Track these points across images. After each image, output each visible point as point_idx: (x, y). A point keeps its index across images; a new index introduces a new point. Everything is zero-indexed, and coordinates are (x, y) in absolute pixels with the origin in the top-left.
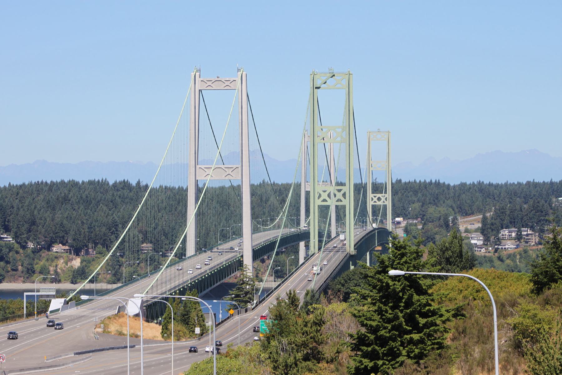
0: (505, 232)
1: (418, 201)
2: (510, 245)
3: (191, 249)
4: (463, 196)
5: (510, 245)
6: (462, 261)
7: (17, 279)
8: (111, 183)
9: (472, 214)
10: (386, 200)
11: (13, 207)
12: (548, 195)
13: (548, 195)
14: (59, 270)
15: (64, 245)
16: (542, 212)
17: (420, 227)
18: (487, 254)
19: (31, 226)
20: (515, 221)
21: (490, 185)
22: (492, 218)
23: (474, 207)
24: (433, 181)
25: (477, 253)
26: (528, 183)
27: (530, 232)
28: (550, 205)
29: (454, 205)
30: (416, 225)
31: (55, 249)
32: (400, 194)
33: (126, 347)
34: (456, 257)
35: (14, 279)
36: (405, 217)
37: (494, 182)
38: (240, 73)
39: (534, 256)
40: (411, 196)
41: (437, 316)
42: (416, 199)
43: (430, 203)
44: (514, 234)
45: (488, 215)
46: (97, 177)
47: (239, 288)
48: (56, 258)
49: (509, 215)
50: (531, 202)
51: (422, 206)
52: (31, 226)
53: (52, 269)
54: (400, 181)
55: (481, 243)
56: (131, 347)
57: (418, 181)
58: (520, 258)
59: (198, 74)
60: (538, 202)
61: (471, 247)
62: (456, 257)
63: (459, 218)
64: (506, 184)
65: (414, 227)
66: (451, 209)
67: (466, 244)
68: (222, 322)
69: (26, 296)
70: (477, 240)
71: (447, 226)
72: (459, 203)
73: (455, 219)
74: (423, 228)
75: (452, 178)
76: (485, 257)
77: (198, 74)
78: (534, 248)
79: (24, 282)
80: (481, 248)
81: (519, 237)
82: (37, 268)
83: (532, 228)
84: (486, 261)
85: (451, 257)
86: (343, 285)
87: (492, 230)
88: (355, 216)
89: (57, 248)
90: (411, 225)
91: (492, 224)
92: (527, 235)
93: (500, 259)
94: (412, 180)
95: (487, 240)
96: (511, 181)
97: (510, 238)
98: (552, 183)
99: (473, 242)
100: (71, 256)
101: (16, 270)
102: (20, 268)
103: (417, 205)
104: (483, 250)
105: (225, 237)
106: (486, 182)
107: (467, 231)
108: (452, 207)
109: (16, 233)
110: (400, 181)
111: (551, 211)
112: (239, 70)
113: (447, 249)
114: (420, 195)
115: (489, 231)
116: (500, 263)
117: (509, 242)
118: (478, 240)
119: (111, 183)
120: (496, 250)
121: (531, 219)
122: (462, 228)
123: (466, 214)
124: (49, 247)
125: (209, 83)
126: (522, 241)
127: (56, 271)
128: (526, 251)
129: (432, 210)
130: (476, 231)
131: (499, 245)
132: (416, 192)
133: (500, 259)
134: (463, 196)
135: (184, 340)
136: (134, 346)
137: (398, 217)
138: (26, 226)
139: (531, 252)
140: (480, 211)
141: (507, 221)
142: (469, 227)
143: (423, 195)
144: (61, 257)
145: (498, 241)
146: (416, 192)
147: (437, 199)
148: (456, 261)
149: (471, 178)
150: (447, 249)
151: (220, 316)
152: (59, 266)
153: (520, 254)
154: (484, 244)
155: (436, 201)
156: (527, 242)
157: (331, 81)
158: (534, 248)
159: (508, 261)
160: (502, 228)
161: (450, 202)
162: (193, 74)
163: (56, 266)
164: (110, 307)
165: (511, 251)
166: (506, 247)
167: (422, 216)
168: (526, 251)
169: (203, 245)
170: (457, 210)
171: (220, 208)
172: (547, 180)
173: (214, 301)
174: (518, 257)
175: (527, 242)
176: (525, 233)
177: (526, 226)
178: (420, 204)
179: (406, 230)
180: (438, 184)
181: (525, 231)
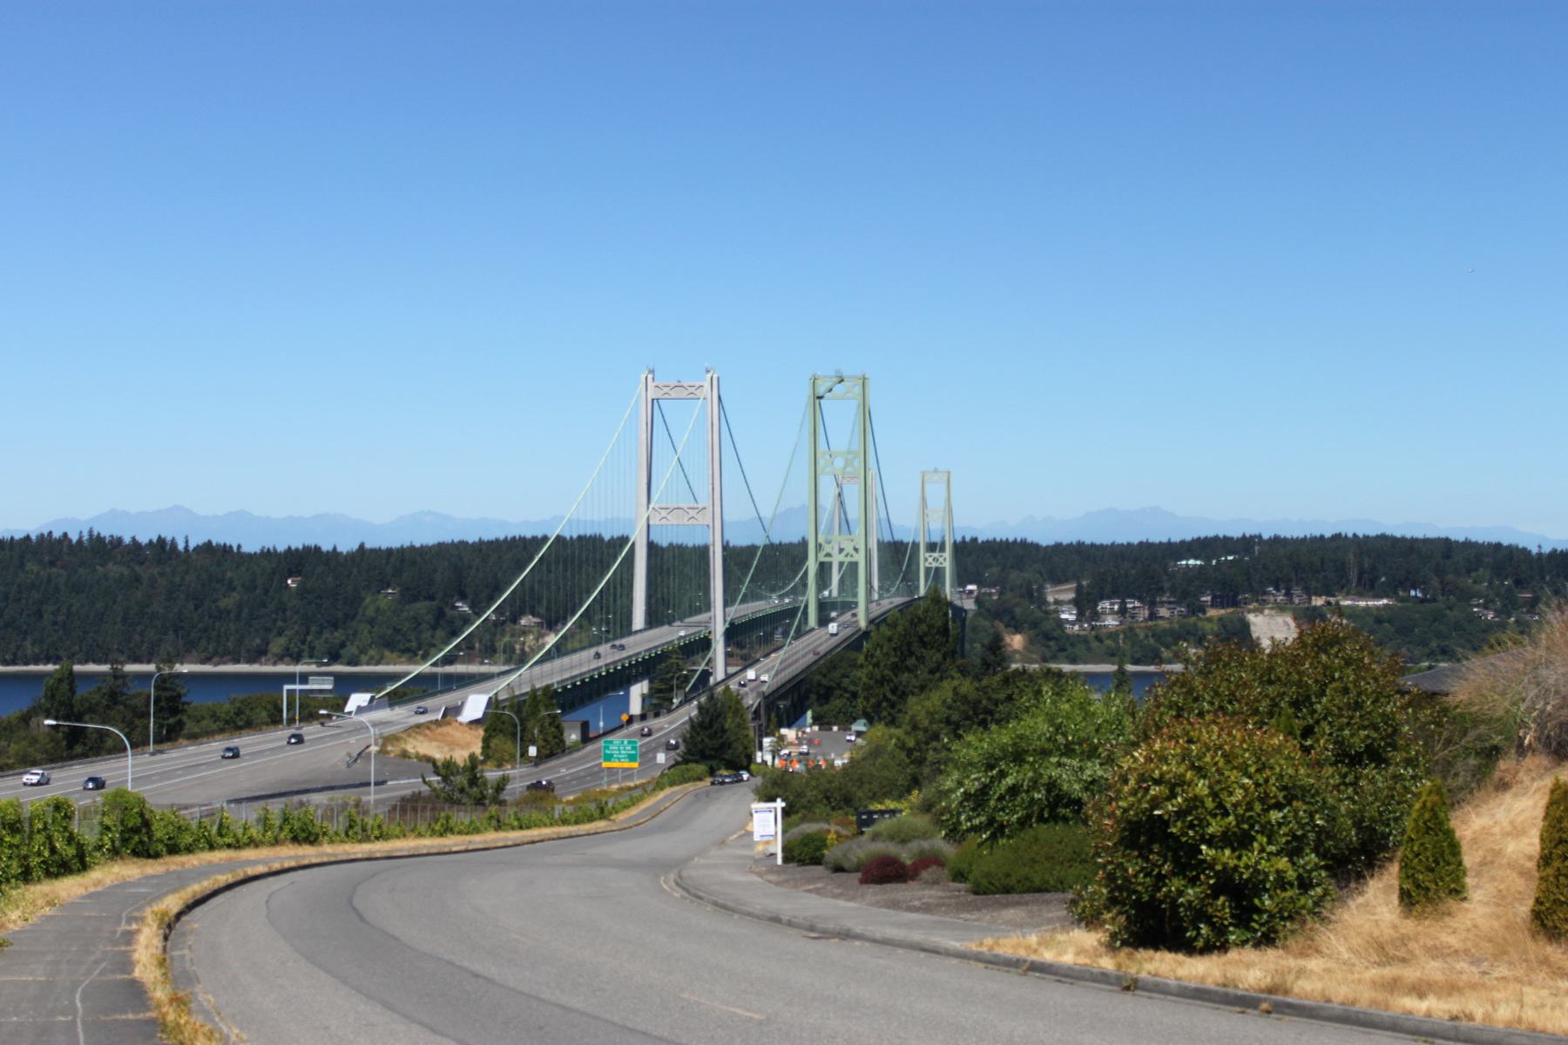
0: (1105, 605)
2: (1111, 622)
3: (639, 620)
5: (1111, 622)
10: (946, 560)
27: (1137, 604)
31: (523, 622)
33: (369, 784)
37: (1098, 542)
39: (1142, 636)
40: (976, 557)
41: (117, 843)
63: (1251, 617)
70: (1068, 615)
71: (1030, 595)
75: (1044, 537)
81: (1123, 611)
82: (500, 645)
83: (1140, 599)
85: (926, 634)
95: (1080, 615)
97: (1112, 612)
99: (1063, 616)
103: (995, 570)
105: (699, 611)
106: (1088, 541)
107: (1057, 602)
113: (921, 620)
115: (1085, 604)
120: (1093, 628)
122: (1050, 599)
124: (515, 620)
128: (1131, 629)
129: (1015, 577)
130: (1069, 602)
136: (383, 783)
145: (1096, 616)
150: (921, 620)
155: (1020, 564)
159: (1108, 642)
160: (1102, 599)
167: (1000, 582)
168: (1131, 629)
169: (653, 620)
171: (677, 569)
172: (1164, 540)
173: (1442, 664)
177: (1133, 596)
180: (1024, 544)
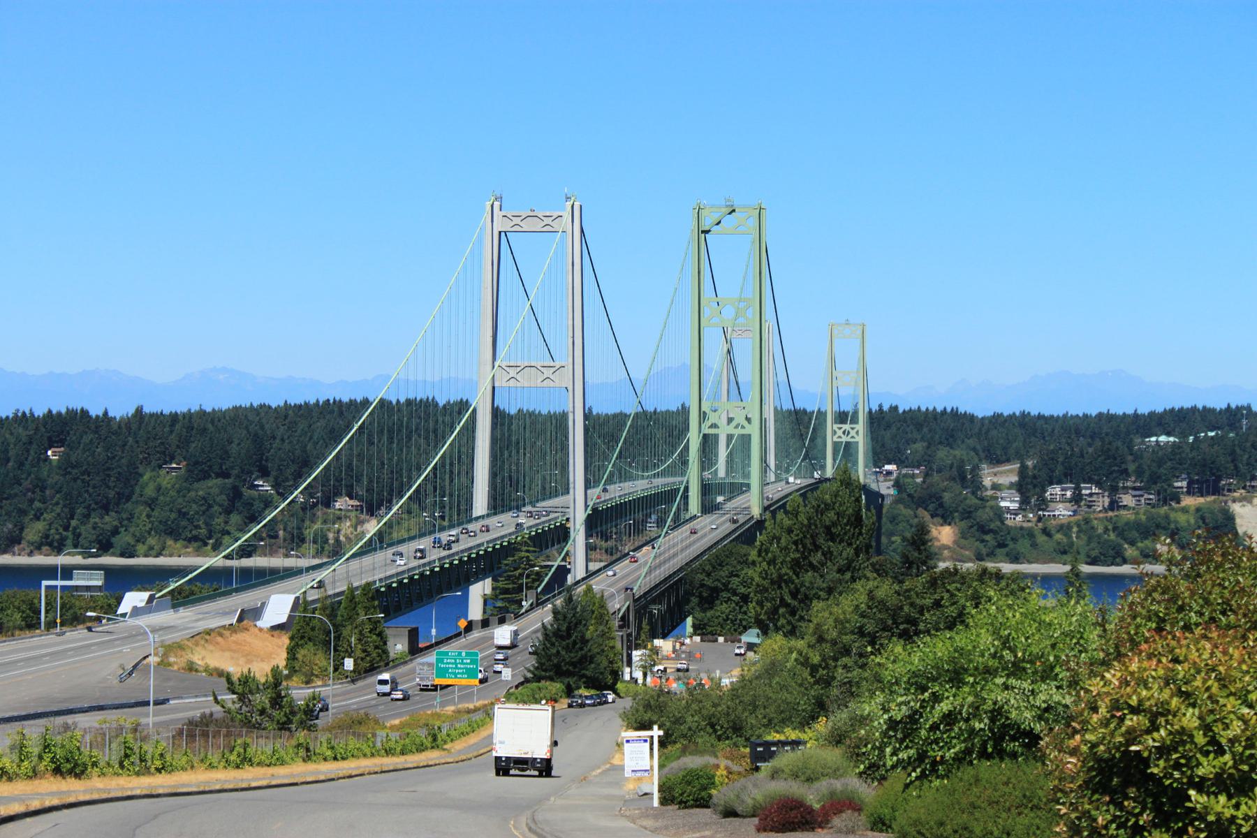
0: (1055, 490)
1: (922, 439)
2: (1062, 511)
4: (994, 433)
5: (1062, 511)
6: (860, 534)
7: (276, 552)
8: (441, 403)
9: (1008, 461)
10: (859, 434)
11: (274, 438)
12: (1128, 433)
13: (1128, 433)
14: (342, 538)
15: (351, 498)
16: (1115, 459)
17: (919, 480)
18: (1025, 525)
19: (301, 468)
20: (1072, 473)
21: (1040, 417)
22: (1035, 467)
23: (1011, 451)
24: (949, 410)
25: (1009, 523)
26: (1100, 415)
27: (1095, 490)
28: (1130, 448)
29: (978, 447)
30: (913, 476)
31: (338, 505)
32: (894, 429)
34: (846, 525)
35: (272, 553)
36: (900, 463)
38: (569, 204)
40: (894, 430)
42: (919, 437)
43: (941, 443)
44: (1069, 494)
45: (1030, 463)
46: (420, 394)
47: (509, 577)
48: (339, 518)
49: (1063, 463)
50: (1098, 443)
51: (928, 447)
52: (301, 468)
53: (331, 535)
54: (896, 408)
55: (1016, 506)
56: (157, 703)
57: (923, 409)
58: (1079, 532)
59: (497, 204)
60: (1110, 443)
61: (999, 513)
62: (846, 525)
63: (1236, 508)
64: (1065, 416)
65: (909, 480)
66: (973, 453)
67: (992, 507)
68: (438, 644)
69: (47, 587)
70: (1009, 502)
71: (963, 478)
72: (986, 443)
73: (976, 469)
74: (924, 482)
76: (1022, 528)
77: (497, 204)
78: (1101, 515)
79: (287, 556)
80: (1016, 515)
81: (1077, 499)
82: (309, 533)
83: (1099, 484)
84: (1023, 536)
86: (709, 575)
87: (1035, 486)
88: (834, 460)
89: (342, 503)
90: (905, 476)
91: (1035, 477)
92: (1091, 495)
93: (1046, 532)
94: (914, 407)
95: (1024, 502)
96: (1073, 412)
97: (1064, 500)
98: (1136, 415)
99: (1003, 504)
100: (363, 517)
101: (276, 537)
102: (281, 533)
103: (919, 446)
104: (1019, 518)
106: (1034, 412)
107: (995, 487)
108: (974, 449)
109: (276, 478)
110: (896, 408)
111: (1130, 458)
112: (568, 198)
113: (828, 507)
114: (925, 430)
115: (1031, 489)
116: (1044, 538)
117: (1061, 505)
118: (1012, 501)
119: (441, 403)
120: (1040, 519)
121: (1097, 469)
122: (987, 482)
123: (996, 461)
124: (327, 503)
125: (517, 221)
126: (1083, 503)
127: (337, 540)
128: (1087, 521)
129: (942, 454)
130: (1011, 486)
131: (1044, 510)
132: (919, 426)
133: (1046, 532)
134: (994, 433)
135: (320, 683)
137: (889, 463)
138: (293, 468)
139: (1095, 522)
140: (1020, 457)
141: (1059, 470)
142: (999, 480)
143: (930, 431)
144: (346, 517)
145: (1043, 504)
146: (919, 426)
147: (952, 436)
148: (845, 534)
149: (1009, 407)
151: (434, 631)
152: (343, 532)
153: (1078, 526)
154: (1020, 508)
155: (950, 439)
156: (1090, 507)
157: (728, 221)
158: (1101, 515)
159: (1058, 536)
160: (1051, 483)
161: (970, 442)
162: (489, 204)
163: (339, 531)
164: (226, 614)
165: (1064, 521)
166: (1057, 513)
167: (926, 461)
168: (1087, 521)
170: (982, 455)
172: (1130, 411)
174: (1075, 529)
175: (1090, 507)
176: (1088, 492)
177: (1090, 481)
178: (925, 444)
179: (897, 485)
180: (955, 414)
181: (1086, 488)
